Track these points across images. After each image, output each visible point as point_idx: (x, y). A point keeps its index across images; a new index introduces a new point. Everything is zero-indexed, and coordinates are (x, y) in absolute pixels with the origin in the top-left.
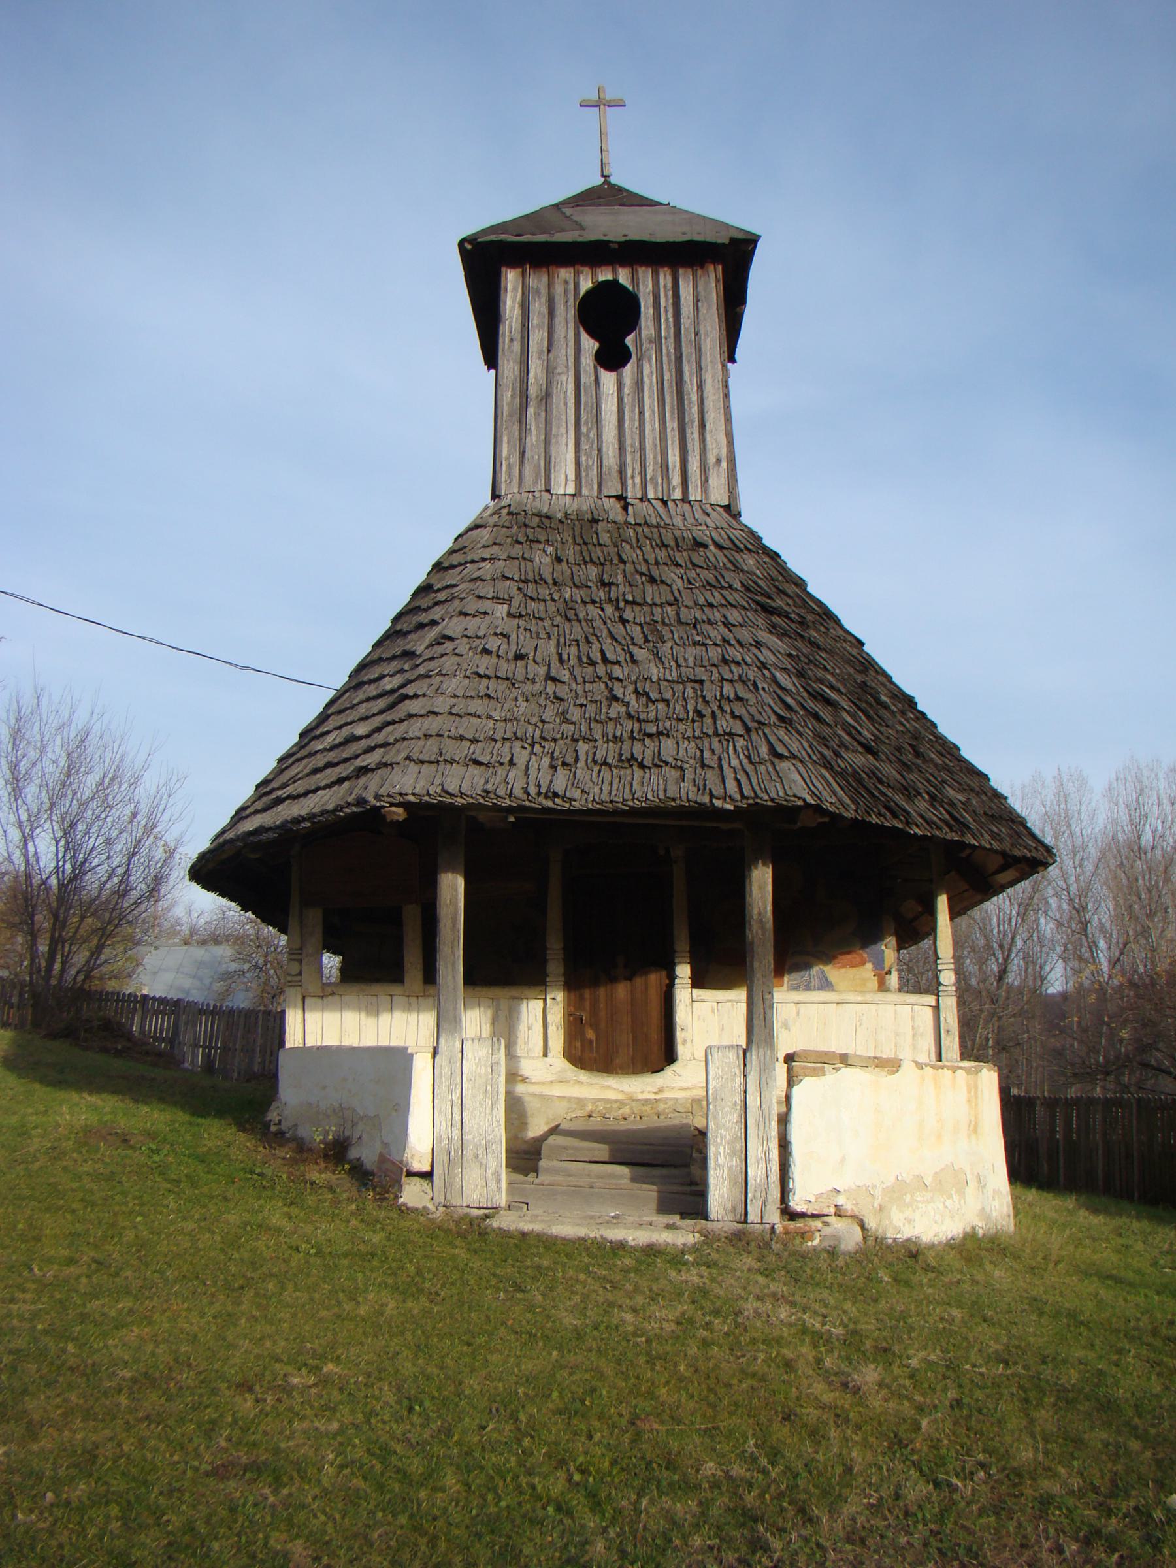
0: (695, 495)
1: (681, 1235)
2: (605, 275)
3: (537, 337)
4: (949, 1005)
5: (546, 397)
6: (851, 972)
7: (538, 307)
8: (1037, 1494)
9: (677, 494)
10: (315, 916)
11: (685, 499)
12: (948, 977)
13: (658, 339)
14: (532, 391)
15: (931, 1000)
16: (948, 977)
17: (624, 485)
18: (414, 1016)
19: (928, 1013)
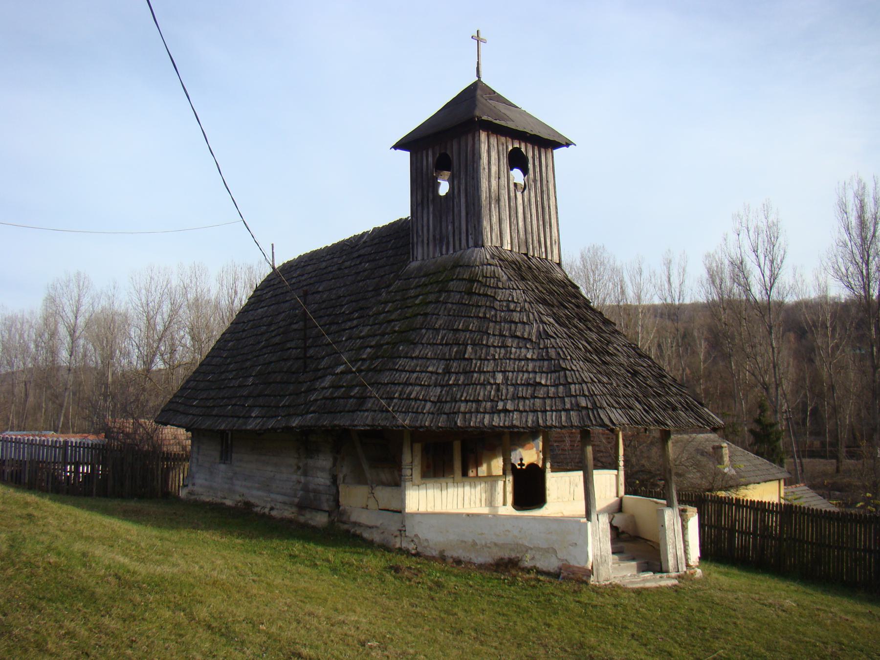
0: (549, 258)
1: (650, 580)
2: (517, 145)
3: (494, 169)
4: (622, 473)
5: (498, 200)
6: (529, 451)
7: (494, 155)
8: (230, 624)
9: (544, 257)
10: (418, 447)
11: (546, 259)
12: (621, 463)
13: (535, 181)
14: (493, 196)
15: (615, 472)
16: (621, 463)
17: (528, 249)
18: (460, 490)
19: (614, 477)
